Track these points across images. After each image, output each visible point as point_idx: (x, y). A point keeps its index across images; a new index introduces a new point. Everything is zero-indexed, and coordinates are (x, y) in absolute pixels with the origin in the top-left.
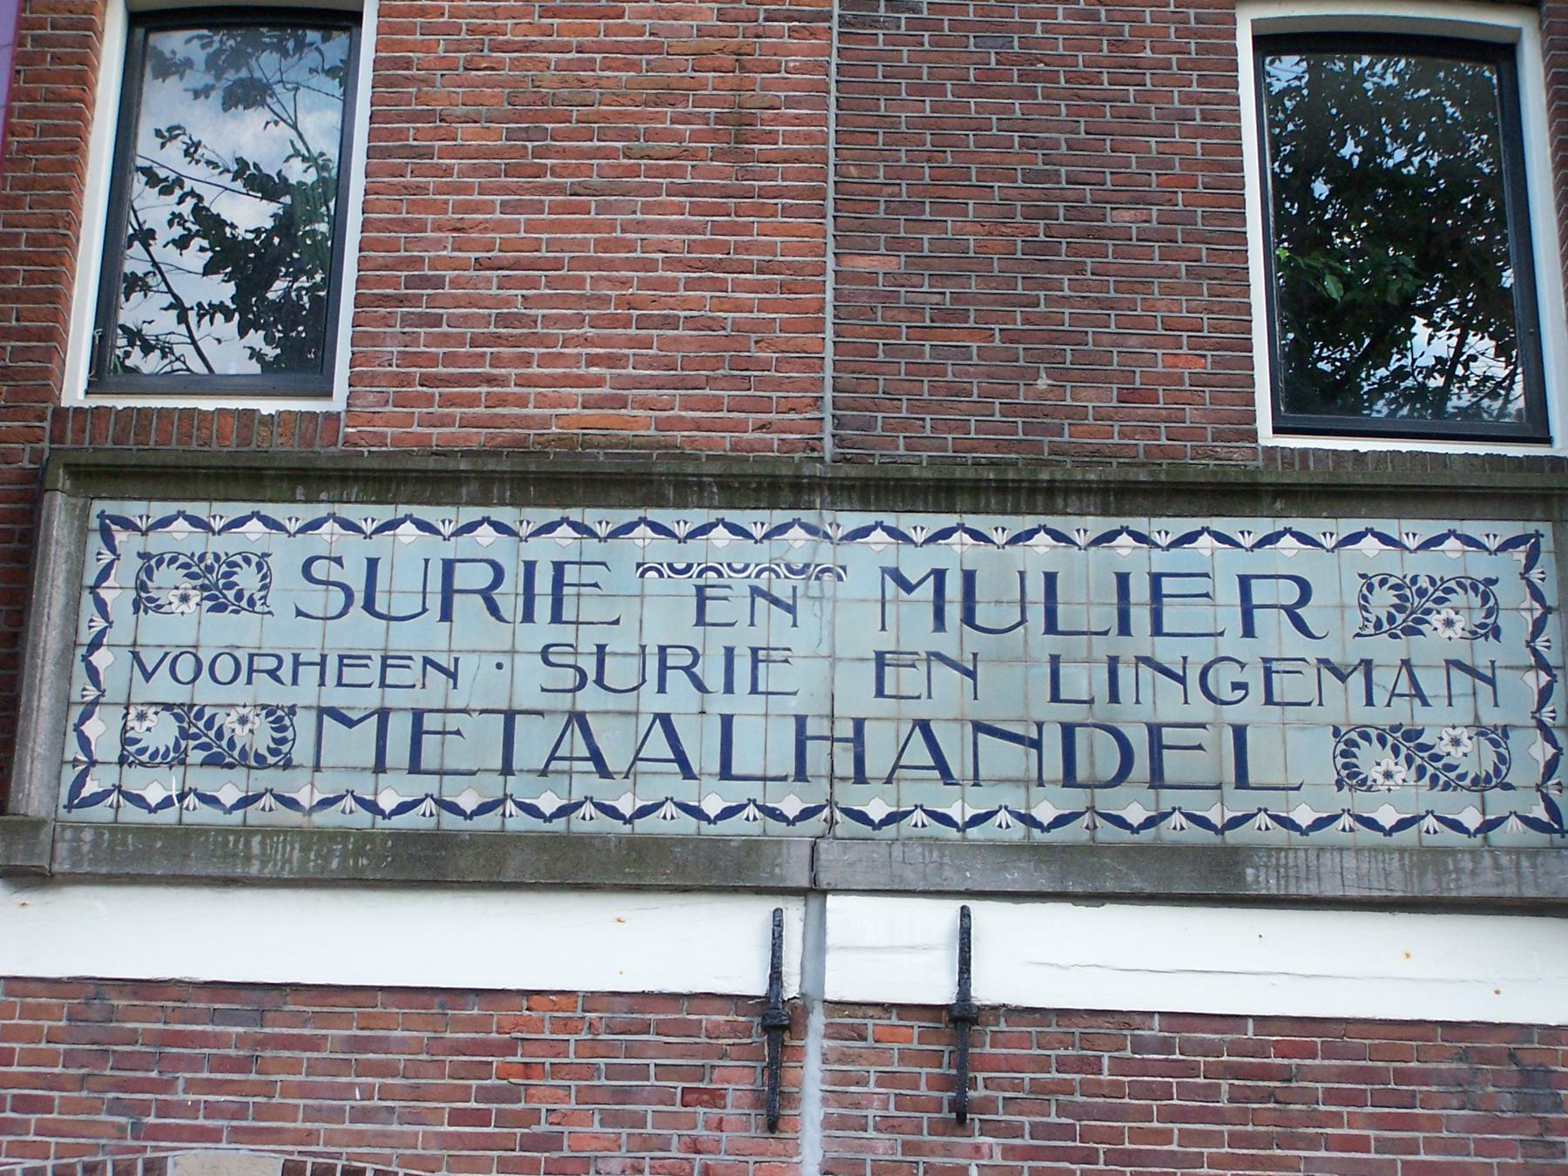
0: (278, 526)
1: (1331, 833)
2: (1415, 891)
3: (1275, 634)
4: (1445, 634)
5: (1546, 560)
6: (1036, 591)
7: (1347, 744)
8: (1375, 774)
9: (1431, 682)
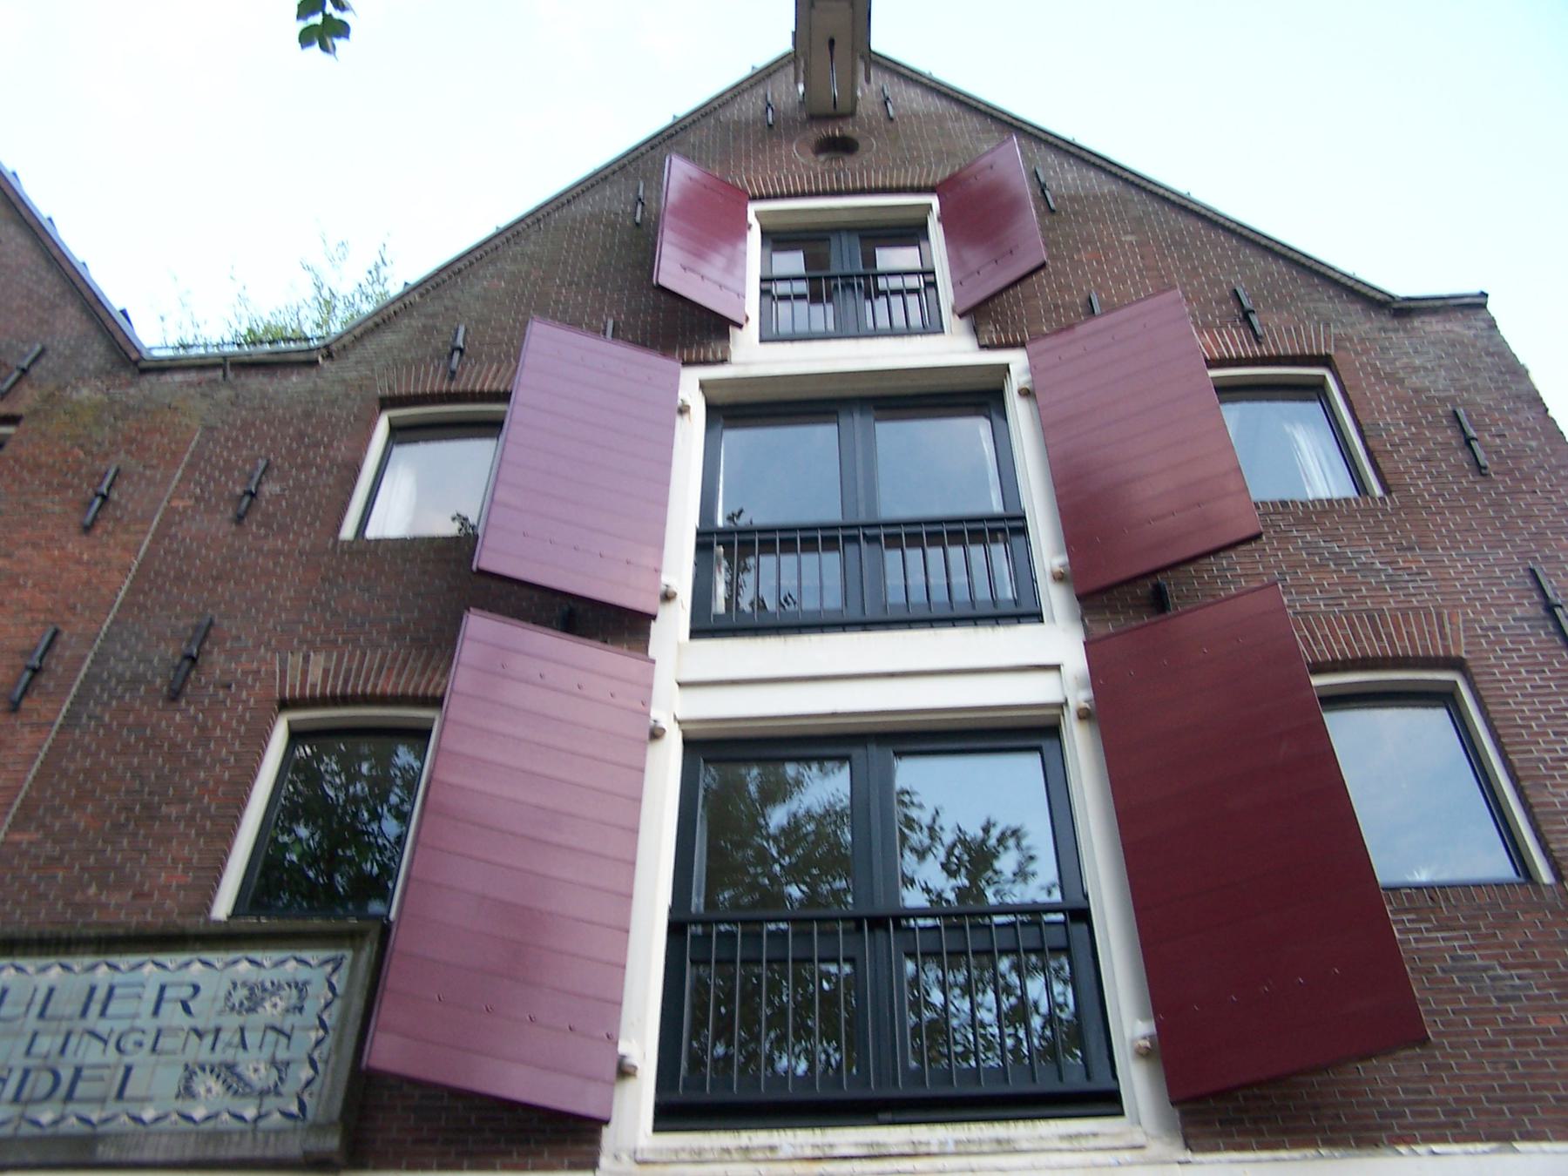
0: (305, 963)
1: (165, 1124)
2: (200, 1155)
3: (172, 1014)
4: (270, 1011)
5: (344, 971)
6: (40, 997)
7: (189, 1073)
8: (201, 1090)
9: (252, 1038)
